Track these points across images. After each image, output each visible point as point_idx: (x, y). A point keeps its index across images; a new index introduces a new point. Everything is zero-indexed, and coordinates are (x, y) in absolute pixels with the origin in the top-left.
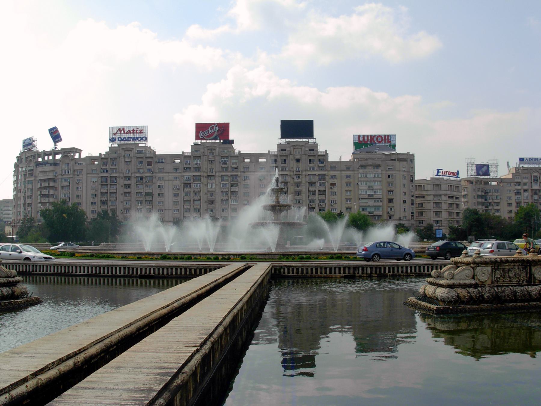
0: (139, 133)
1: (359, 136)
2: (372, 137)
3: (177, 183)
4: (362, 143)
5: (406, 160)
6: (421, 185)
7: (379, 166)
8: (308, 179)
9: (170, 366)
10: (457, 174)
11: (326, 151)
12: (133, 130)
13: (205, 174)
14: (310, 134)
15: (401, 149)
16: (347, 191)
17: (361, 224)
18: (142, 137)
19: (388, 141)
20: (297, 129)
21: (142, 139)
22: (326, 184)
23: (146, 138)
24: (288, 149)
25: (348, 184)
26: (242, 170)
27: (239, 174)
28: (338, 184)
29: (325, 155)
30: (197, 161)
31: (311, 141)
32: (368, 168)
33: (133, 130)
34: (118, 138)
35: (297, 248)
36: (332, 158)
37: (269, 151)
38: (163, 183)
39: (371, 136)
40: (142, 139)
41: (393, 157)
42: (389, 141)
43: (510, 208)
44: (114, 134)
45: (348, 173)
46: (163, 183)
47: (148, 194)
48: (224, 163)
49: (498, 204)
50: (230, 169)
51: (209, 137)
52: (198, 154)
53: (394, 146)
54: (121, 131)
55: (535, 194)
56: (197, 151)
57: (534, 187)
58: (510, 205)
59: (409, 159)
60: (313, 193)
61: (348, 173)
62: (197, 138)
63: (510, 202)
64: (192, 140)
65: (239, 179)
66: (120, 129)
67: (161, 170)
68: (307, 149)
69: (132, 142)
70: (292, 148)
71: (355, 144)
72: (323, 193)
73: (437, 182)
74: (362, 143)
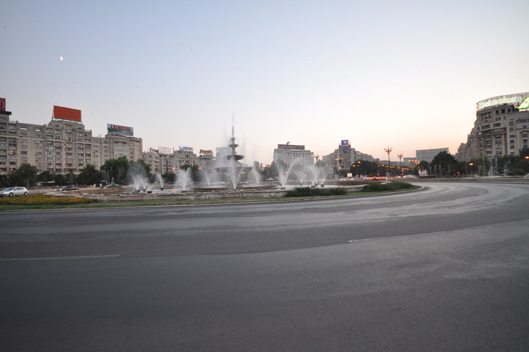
1: (111, 125)
2: (120, 127)
5: (139, 142)
6: (144, 155)
7: (126, 143)
8: (77, 146)
10: (158, 151)
11: (91, 131)
15: (136, 135)
16: (105, 155)
17: (301, 185)
19: (129, 130)
26: (20, 135)
27: (17, 137)
29: (90, 133)
31: (79, 123)
32: (120, 144)
35: (469, 203)
36: (94, 135)
37: (17, 122)
41: (132, 139)
42: (129, 131)
45: (106, 145)
50: (7, 132)
52: (51, 127)
53: (132, 134)
59: (139, 141)
65: (17, 141)
68: (55, 125)
70: (64, 126)
71: (108, 129)
73: (150, 154)
74: (112, 129)
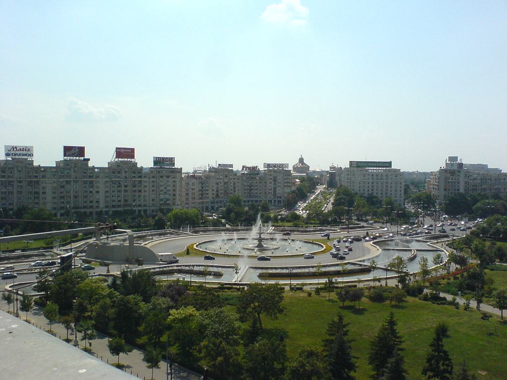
0: (28, 151)
3: (55, 185)
4: (158, 161)
9: (365, 282)
12: (23, 149)
13: (73, 180)
14: (133, 157)
18: (30, 153)
19: (171, 161)
20: (125, 153)
21: (30, 155)
22: (142, 186)
23: (33, 155)
24: (121, 165)
25: (153, 186)
28: (148, 186)
30: (67, 171)
33: (23, 149)
34: (12, 154)
38: (45, 185)
39: (163, 158)
40: (30, 155)
43: (213, 192)
44: (9, 151)
45: (153, 180)
46: (45, 185)
47: (36, 193)
48: (85, 173)
49: (207, 190)
51: (73, 155)
54: (14, 149)
55: (225, 184)
56: (67, 165)
57: (225, 181)
58: (213, 190)
60: (135, 191)
61: (153, 180)
62: (65, 155)
63: (213, 189)
64: (61, 157)
66: (13, 147)
67: (43, 177)
69: (24, 157)
72: (140, 191)
